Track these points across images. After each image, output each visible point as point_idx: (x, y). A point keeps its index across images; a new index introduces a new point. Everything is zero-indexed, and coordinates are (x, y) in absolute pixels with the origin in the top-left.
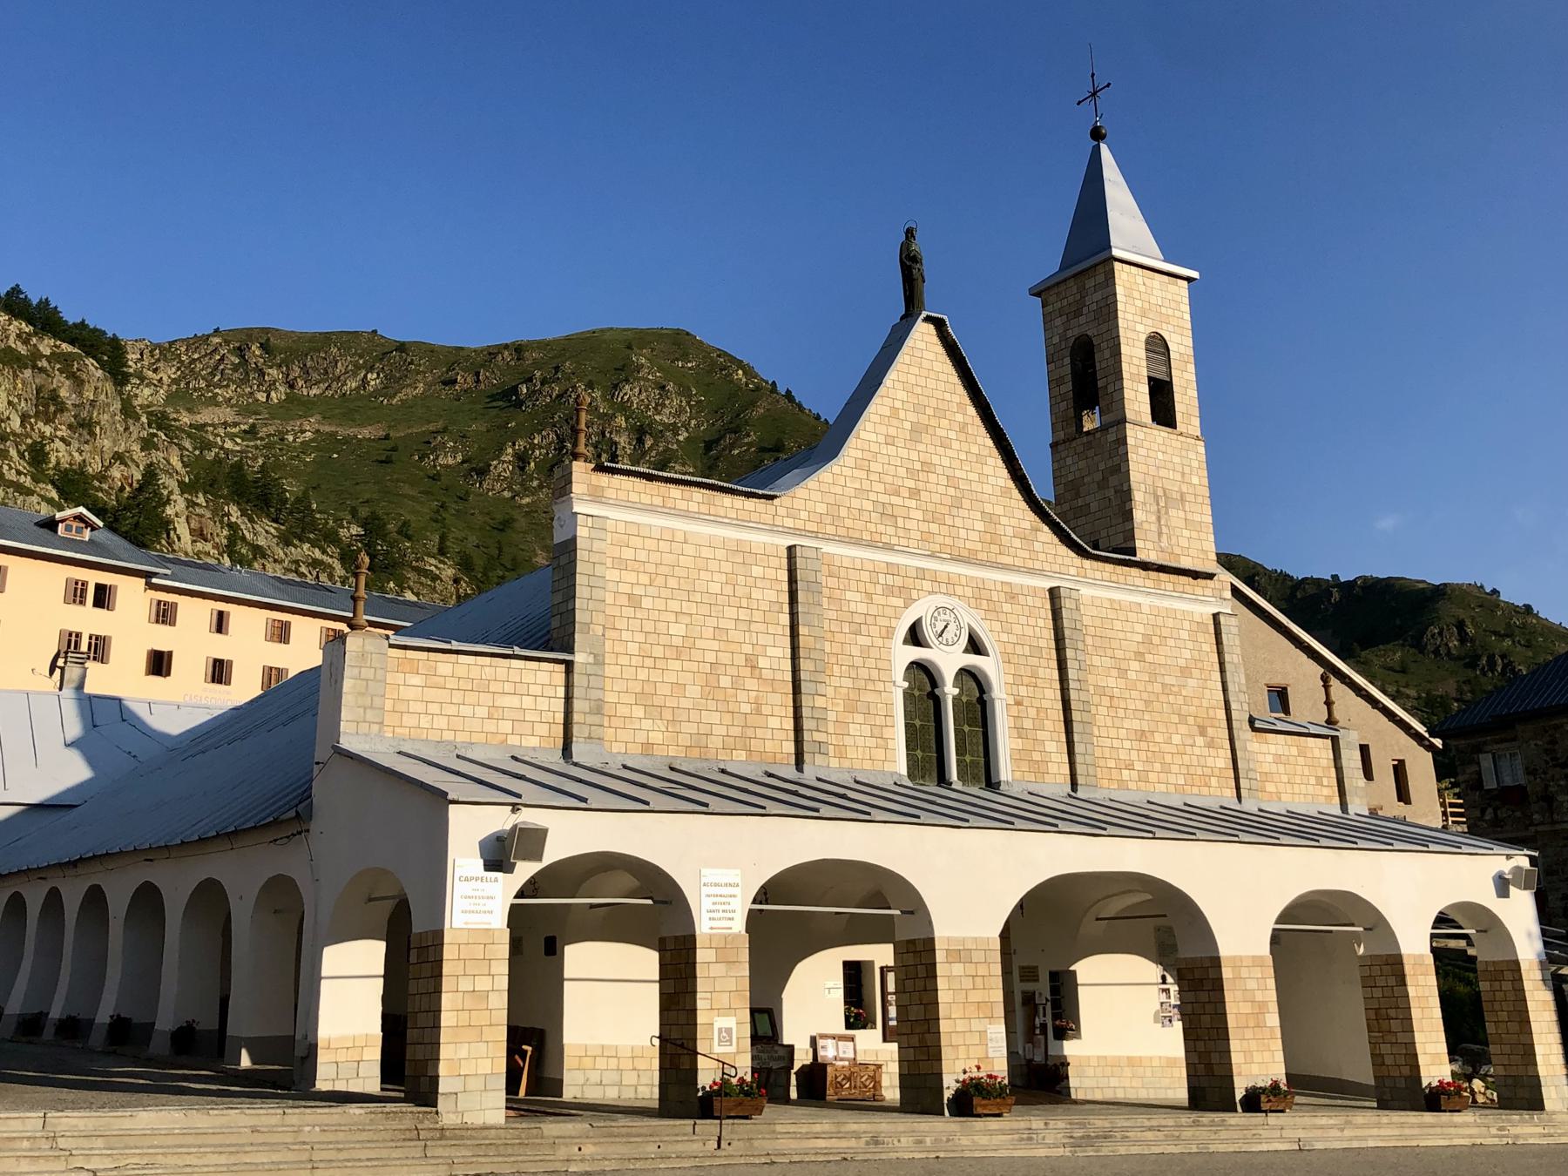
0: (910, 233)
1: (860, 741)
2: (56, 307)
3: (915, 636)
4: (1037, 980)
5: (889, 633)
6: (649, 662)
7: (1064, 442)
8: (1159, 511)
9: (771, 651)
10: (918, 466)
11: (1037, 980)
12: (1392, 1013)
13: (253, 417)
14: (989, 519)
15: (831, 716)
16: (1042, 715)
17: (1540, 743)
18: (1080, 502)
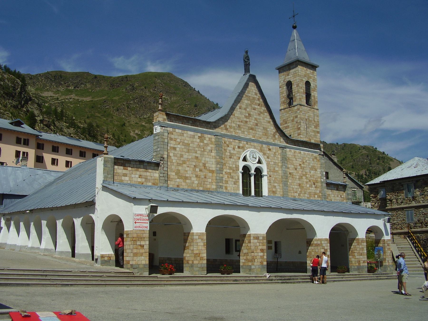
0: (247, 52)
1: (231, 185)
2: (376, 148)
3: (245, 159)
4: (272, 244)
5: (239, 158)
7: (283, 109)
8: (307, 128)
9: (209, 162)
10: (247, 115)
11: (272, 244)
12: (355, 251)
13: (58, 95)
14: (265, 129)
15: (224, 179)
16: (276, 179)
17: (390, 187)
18: (287, 125)
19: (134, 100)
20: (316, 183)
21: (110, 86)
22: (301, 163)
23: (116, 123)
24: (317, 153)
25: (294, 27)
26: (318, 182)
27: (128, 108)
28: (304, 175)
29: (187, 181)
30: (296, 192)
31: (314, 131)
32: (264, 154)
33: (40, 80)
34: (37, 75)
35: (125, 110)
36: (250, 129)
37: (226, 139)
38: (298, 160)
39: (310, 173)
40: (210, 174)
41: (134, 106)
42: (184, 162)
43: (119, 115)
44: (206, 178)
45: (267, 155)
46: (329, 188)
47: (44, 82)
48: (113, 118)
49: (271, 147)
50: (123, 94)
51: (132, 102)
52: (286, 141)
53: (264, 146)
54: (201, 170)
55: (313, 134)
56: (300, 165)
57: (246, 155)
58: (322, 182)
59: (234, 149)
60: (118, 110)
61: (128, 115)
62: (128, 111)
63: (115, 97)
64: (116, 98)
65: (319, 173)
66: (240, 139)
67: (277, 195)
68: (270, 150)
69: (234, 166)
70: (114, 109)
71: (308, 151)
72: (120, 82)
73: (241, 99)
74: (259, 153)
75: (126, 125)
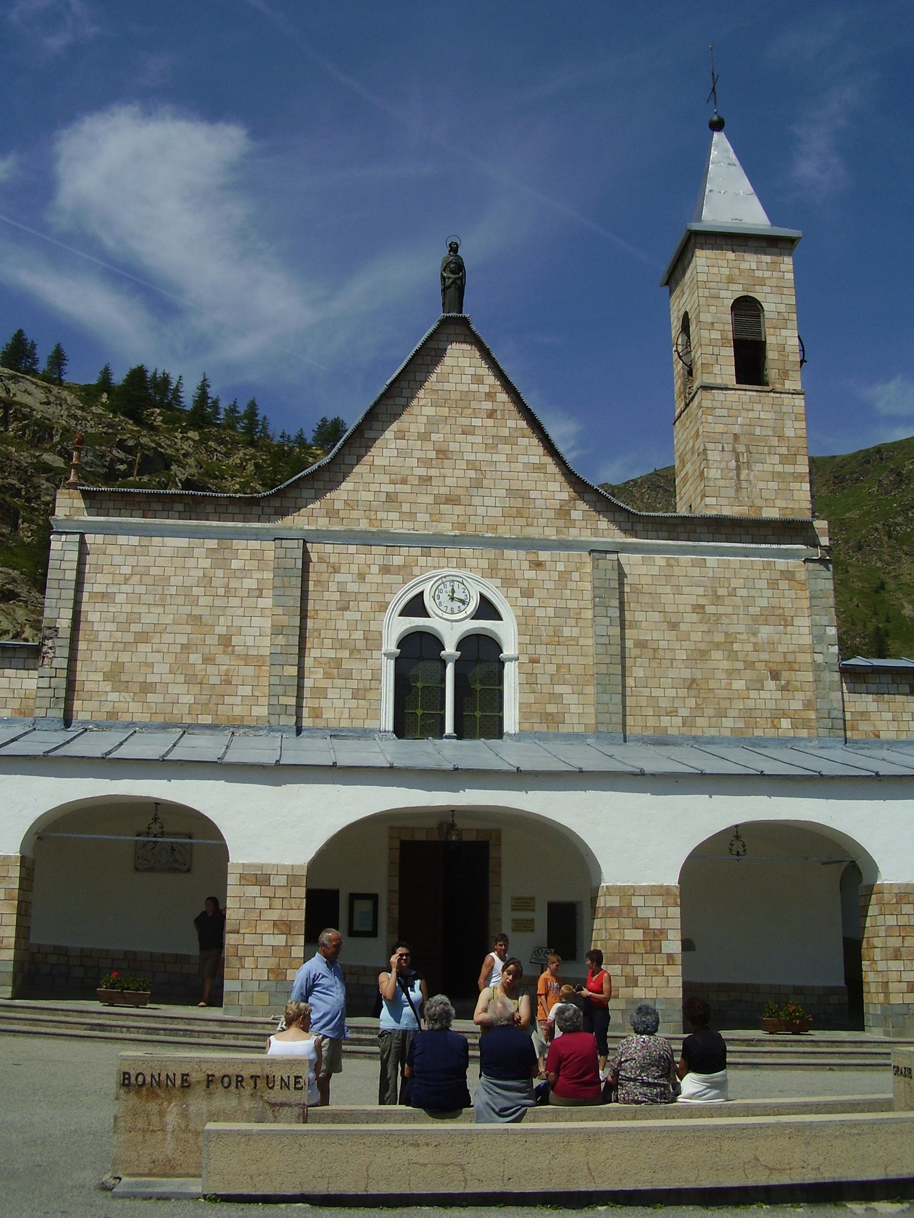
0: (454, 248)
4: (533, 910)
6: (121, 646)
8: (738, 468)
11: (533, 910)
19: (905, 511)
20: (785, 675)
21: (834, 483)
22: (702, 601)
23: (858, 585)
24: (798, 557)
25: (717, 126)
26: (796, 667)
27: (890, 537)
28: (718, 646)
29: (150, 697)
30: (672, 713)
31: (777, 476)
32: (508, 582)
33: (637, 495)
34: (628, 482)
35: (881, 546)
36: (444, 501)
37: (329, 548)
38: (686, 590)
39: (755, 634)
40: (250, 671)
41: (909, 530)
42: (143, 637)
43: (866, 562)
44: (230, 683)
45: (524, 584)
46: (859, 687)
47: (648, 499)
48: (847, 572)
49: (544, 556)
50: (871, 500)
51: (900, 519)
52: (628, 526)
53: (510, 554)
54: (208, 660)
55: (773, 485)
56: (698, 608)
57: (422, 593)
58: (817, 668)
59: (362, 577)
60: (860, 548)
61: (893, 558)
62: (890, 547)
63: (849, 510)
64: (854, 514)
65: (806, 630)
66: (391, 541)
67: (564, 729)
68: (538, 565)
69: (359, 635)
70: (850, 545)
71: (746, 553)
72: (860, 468)
73: (407, 405)
74: (482, 580)
75: (887, 587)
